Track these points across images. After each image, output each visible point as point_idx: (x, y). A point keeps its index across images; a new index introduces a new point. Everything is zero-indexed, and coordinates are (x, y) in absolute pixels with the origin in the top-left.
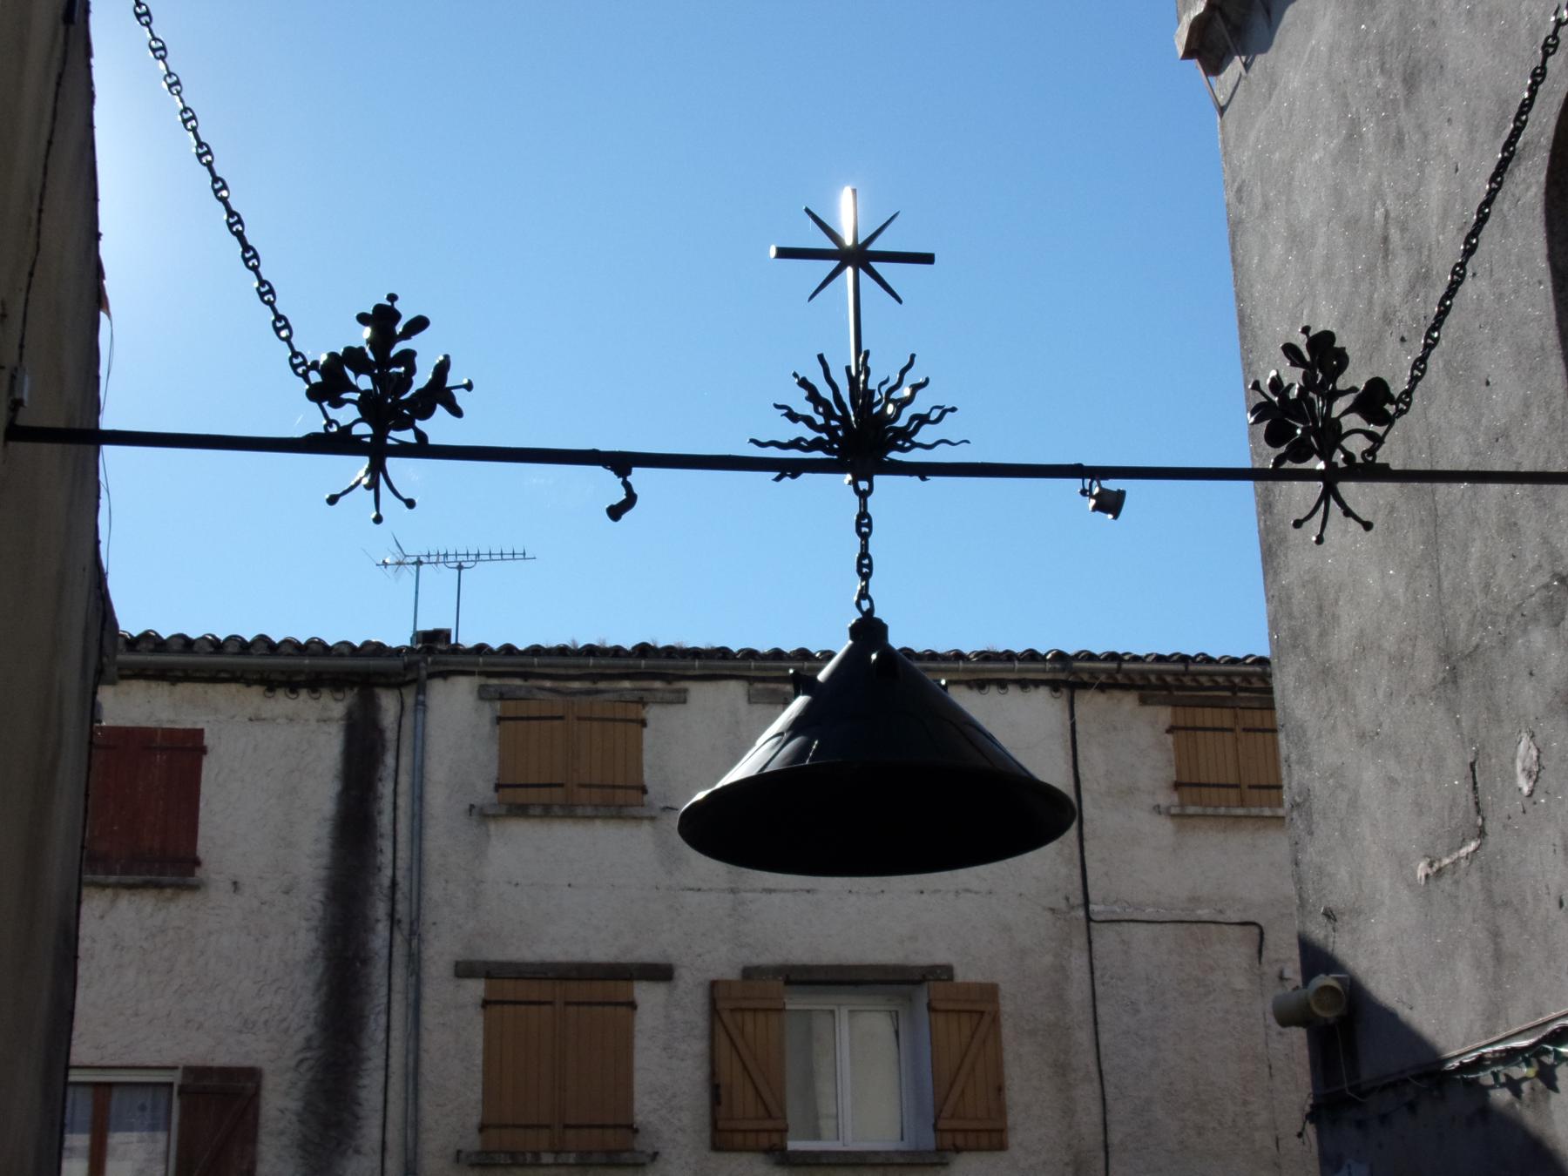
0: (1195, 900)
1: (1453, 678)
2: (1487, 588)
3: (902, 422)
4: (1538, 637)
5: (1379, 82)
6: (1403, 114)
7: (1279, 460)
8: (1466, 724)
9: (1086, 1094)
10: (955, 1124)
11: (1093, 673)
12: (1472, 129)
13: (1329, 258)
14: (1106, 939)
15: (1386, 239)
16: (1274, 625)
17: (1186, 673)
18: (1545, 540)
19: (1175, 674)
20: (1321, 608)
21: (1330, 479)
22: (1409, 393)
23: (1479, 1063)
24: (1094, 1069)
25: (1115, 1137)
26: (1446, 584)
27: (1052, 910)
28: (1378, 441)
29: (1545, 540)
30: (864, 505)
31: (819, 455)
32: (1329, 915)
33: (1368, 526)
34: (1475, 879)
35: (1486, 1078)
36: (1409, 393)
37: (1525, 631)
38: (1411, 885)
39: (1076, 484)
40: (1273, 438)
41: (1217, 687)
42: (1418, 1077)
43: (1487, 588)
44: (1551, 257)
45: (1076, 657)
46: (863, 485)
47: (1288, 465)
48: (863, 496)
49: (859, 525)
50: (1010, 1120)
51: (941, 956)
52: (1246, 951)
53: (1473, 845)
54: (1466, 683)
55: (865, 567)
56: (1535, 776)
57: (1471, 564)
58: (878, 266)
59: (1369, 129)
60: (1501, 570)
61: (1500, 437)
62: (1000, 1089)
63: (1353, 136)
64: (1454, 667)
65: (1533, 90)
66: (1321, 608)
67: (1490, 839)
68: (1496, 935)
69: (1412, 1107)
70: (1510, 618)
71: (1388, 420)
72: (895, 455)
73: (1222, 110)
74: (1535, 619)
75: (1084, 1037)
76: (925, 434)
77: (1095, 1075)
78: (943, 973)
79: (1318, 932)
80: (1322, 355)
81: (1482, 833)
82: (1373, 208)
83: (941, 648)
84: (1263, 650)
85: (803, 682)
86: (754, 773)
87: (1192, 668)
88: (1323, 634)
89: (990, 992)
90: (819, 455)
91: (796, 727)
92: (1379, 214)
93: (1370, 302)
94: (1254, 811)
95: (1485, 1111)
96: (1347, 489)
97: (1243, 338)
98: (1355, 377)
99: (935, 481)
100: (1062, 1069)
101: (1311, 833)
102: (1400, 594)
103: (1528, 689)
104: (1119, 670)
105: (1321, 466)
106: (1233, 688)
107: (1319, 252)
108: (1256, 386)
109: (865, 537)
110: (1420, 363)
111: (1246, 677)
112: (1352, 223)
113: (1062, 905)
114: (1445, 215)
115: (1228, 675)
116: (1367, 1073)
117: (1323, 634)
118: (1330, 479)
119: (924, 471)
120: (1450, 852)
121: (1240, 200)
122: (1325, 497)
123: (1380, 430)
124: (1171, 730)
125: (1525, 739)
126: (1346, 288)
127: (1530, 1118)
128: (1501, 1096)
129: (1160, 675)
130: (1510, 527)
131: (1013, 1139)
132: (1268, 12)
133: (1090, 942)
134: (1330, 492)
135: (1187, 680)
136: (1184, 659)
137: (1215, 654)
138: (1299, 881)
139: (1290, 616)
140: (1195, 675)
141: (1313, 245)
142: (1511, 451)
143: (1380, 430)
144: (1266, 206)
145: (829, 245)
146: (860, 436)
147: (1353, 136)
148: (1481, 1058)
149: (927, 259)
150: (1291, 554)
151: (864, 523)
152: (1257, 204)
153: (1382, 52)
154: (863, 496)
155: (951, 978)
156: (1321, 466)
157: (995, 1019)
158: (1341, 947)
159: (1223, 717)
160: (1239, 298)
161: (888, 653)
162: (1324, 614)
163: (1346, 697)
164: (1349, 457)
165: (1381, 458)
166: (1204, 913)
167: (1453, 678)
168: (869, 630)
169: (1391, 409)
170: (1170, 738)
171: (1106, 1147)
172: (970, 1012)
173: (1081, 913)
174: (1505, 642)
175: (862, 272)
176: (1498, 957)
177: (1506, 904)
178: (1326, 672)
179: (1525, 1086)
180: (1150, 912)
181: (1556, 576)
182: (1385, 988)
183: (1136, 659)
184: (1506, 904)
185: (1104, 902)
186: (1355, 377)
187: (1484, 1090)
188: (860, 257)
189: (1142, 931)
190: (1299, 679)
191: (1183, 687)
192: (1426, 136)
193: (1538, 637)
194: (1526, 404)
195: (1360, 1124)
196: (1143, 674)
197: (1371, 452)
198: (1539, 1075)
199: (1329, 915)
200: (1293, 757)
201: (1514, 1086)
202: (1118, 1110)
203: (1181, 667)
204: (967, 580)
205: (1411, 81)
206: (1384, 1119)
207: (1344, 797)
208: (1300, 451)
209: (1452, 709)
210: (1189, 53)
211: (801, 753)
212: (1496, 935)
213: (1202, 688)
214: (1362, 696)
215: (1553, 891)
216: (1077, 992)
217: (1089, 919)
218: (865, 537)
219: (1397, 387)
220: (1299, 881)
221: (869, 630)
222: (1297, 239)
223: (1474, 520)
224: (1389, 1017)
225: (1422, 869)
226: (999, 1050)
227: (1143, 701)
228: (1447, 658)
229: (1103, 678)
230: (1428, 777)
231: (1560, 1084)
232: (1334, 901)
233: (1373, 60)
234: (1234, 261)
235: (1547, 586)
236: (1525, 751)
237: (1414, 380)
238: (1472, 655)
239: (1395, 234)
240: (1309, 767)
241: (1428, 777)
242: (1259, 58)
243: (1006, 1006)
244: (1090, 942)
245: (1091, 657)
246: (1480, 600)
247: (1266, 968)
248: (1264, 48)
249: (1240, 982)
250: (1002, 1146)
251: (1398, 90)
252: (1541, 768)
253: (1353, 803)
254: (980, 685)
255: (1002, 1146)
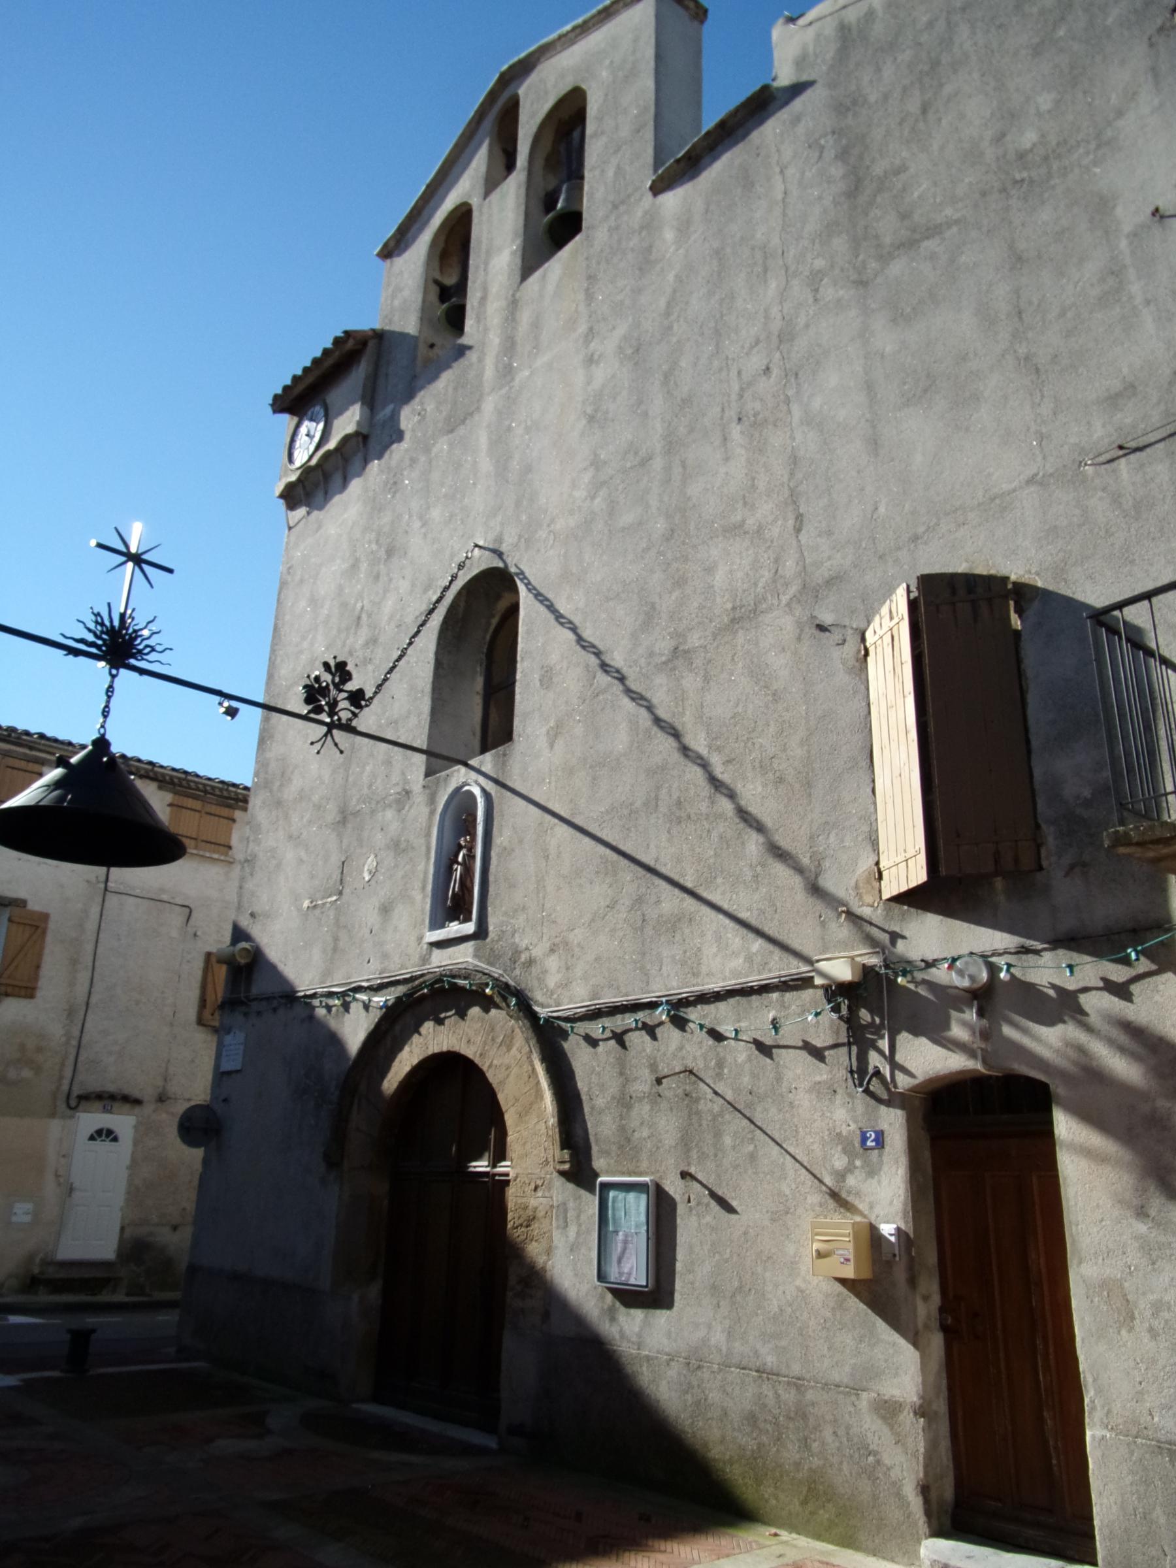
0: (162, 890)
1: (344, 821)
2: (370, 786)
3: (141, 647)
4: (389, 814)
5: (374, 547)
6: (382, 566)
7: (309, 712)
8: (345, 841)
9: (83, 977)
10: (8, 981)
11: (138, 768)
12: (413, 585)
13: (329, 616)
14: (112, 900)
15: (359, 618)
16: (256, 774)
17: (185, 779)
18: (403, 774)
19: (179, 779)
20: (283, 773)
21: (331, 727)
22: (372, 698)
23: (314, 996)
24: (90, 964)
25: (93, 1000)
26: (351, 779)
27: (88, 881)
28: (355, 715)
29: (403, 774)
30: (112, 682)
31: (94, 650)
32: (252, 915)
33: (341, 752)
34: (332, 913)
35: (316, 1002)
36: (372, 698)
37: (384, 810)
38: (299, 909)
39: (217, 699)
40: (308, 701)
41: (198, 789)
42: (281, 997)
43: (370, 786)
44: (437, 653)
45: (132, 759)
46: (114, 672)
47: (312, 715)
48: (113, 677)
49: (108, 691)
50: (40, 984)
51: (21, 894)
52: (183, 919)
53: (334, 898)
54: (350, 826)
55: (105, 713)
56: (373, 874)
57: (366, 774)
58: (145, 566)
59: (364, 566)
60: (379, 781)
61: (394, 723)
62: (38, 967)
63: (355, 566)
64: (345, 817)
65: (451, 582)
66: (283, 773)
67: (345, 897)
68: (336, 939)
69: (275, 1010)
70: (378, 802)
71: (360, 707)
72: (133, 661)
73: (290, 528)
74: (390, 806)
75: (89, 948)
76: (153, 656)
77: (90, 968)
78: (21, 903)
79: (244, 922)
80: (341, 671)
81: (340, 893)
82: (357, 600)
83: (61, 737)
84: (249, 784)
85: (62, 762)
86: (32, 803)
87: (189, 778)
88: (281, 785)
89: (45, 917)
90: (94, 650)
91: (58, 784)
92: (359, 605)
93: (344, 642)
94: (201, 853)
95: (311, 1017)
96: (335, 732)
97: (274, 637)
98: (351, 686)
99: (146, 678)
100: (74, 962)
101: (252, 875)
102: (326, 778)
103: (379, 836)
104: (152, 770)
105: (328, 720)
106: (206, 792)
107: (325, 611)
108: (308, 677)
109: (109, 697)
110: (379, 687)
111: (213, 788)
112: (344, 605)
113: (94, 880)
114: (391, 618)
115: (205, 785)
116: (255, 990)
117: (281, 785)
118: (331, 727)
119: (142, 672)
120: (323, 898)
121: (289, 573)
122: (326, 735)
123: (357, 711)
124: (170, 805)
125: (372, 856)
126: (334, 632)
127: (333, 1023)
128: (321, 1012)
129: (172, 777)
130: (388, 763)
131: (39, 994)
132: (326, 493)
133: (104, 901)
134: (329, 732)
135: (184, 783)
136: (186, 772)
137: (201, 773)
138: (240, 895)
139: (266, 773)
140: (189, 781)
141: (322, 607)
142: (397, 730)
143: (357, 711)
144: (302, 581)
145: (123, 549)
146: (118, 646)
147: (355, 566)
148: (315, 994)
149: (170, 571)
150: (274, 744)
151: (110, 690)
152: (297, 578)
153: (379, 534)
154: (113, 677)
155: (25, 906)
156: (328, 720)
157: (44, 932)
158: (256, 931)
159: (197, 805)
160: (277, 618)
161: (112, 758)
162: (285, 777)
163: (287, 817)
164: (339, 719)
165: (354, 723)
166: (165, 897)
167: (344, 821)
168: (101, 744)
169: (363, 703)
170: (168, 809)
171: (88, 1004)
172: (31, 925)
173: (102, 886)
174: (373, 812)
175: (137, 569)
176: (335, 949)
177: (345, 927)
178: (279, 803)
179: (334, 1009)
180: (138, 892)
181: (404, 790)
182: (273, 954)
183: (162, 767)
184: (345, 927)
185: (116, 882)
186: (351, 686)
187: (314, 1008)
188: (137, 560)
189: (131, 900)
190: (264, 803)
191: (180, 786)
192: (391, 580)
193: (389, 814)
194: (409, 712)
195: (246, 1015)
196: (163, 775)
197: (350, 720)
198: (342, 1005)
199: (252, 915)
200: (252, 838)
201: (329, 1008)
202: (98, 987)
203: (183, 776)
204: (156, 728)
205: (390, 553)
206: (259, 1013)
207: (274, 862)
208: (318, 710)
209: (340, 836)
210: (282, 496)
211: (62, 799)
212: (336, 939)
213: (190, 788)
214: (295, 819)
215: (369, 924)
216: (91, 925)
217: (106, 889)
218: (109, 697)
219: (368, 694)
220: (240, 895)
221: (101, 744)
222: (314, 601)
223: (371, 755)
224: (273, 968)
225: (306, 904)
226: (42, 948)
227: (160, 788)
228: (343, 812)
229: (142, 772)
230: (320, 863)
231: (351, 1011)
232: (257, 909)
233: (373, 536)
234: (278, 600)
235: (398, 793)
236: (371, 862)
237: (376, 693)
238: (356, 814)
239: (364, 617)
240: (259, 845)
241: (320, 863)
242: (315, 513)
243: (52, 925)
244: (104, 901)
245: (139, 760)
246: (365, 791)
247: (189, 929)
248: (321, 508)
249: (174, 934)
250: (32, 996)
251: (382, 553)
252: (377, 871)
253: (278, 866)
254: (141, 777)
255: (32, 996)
